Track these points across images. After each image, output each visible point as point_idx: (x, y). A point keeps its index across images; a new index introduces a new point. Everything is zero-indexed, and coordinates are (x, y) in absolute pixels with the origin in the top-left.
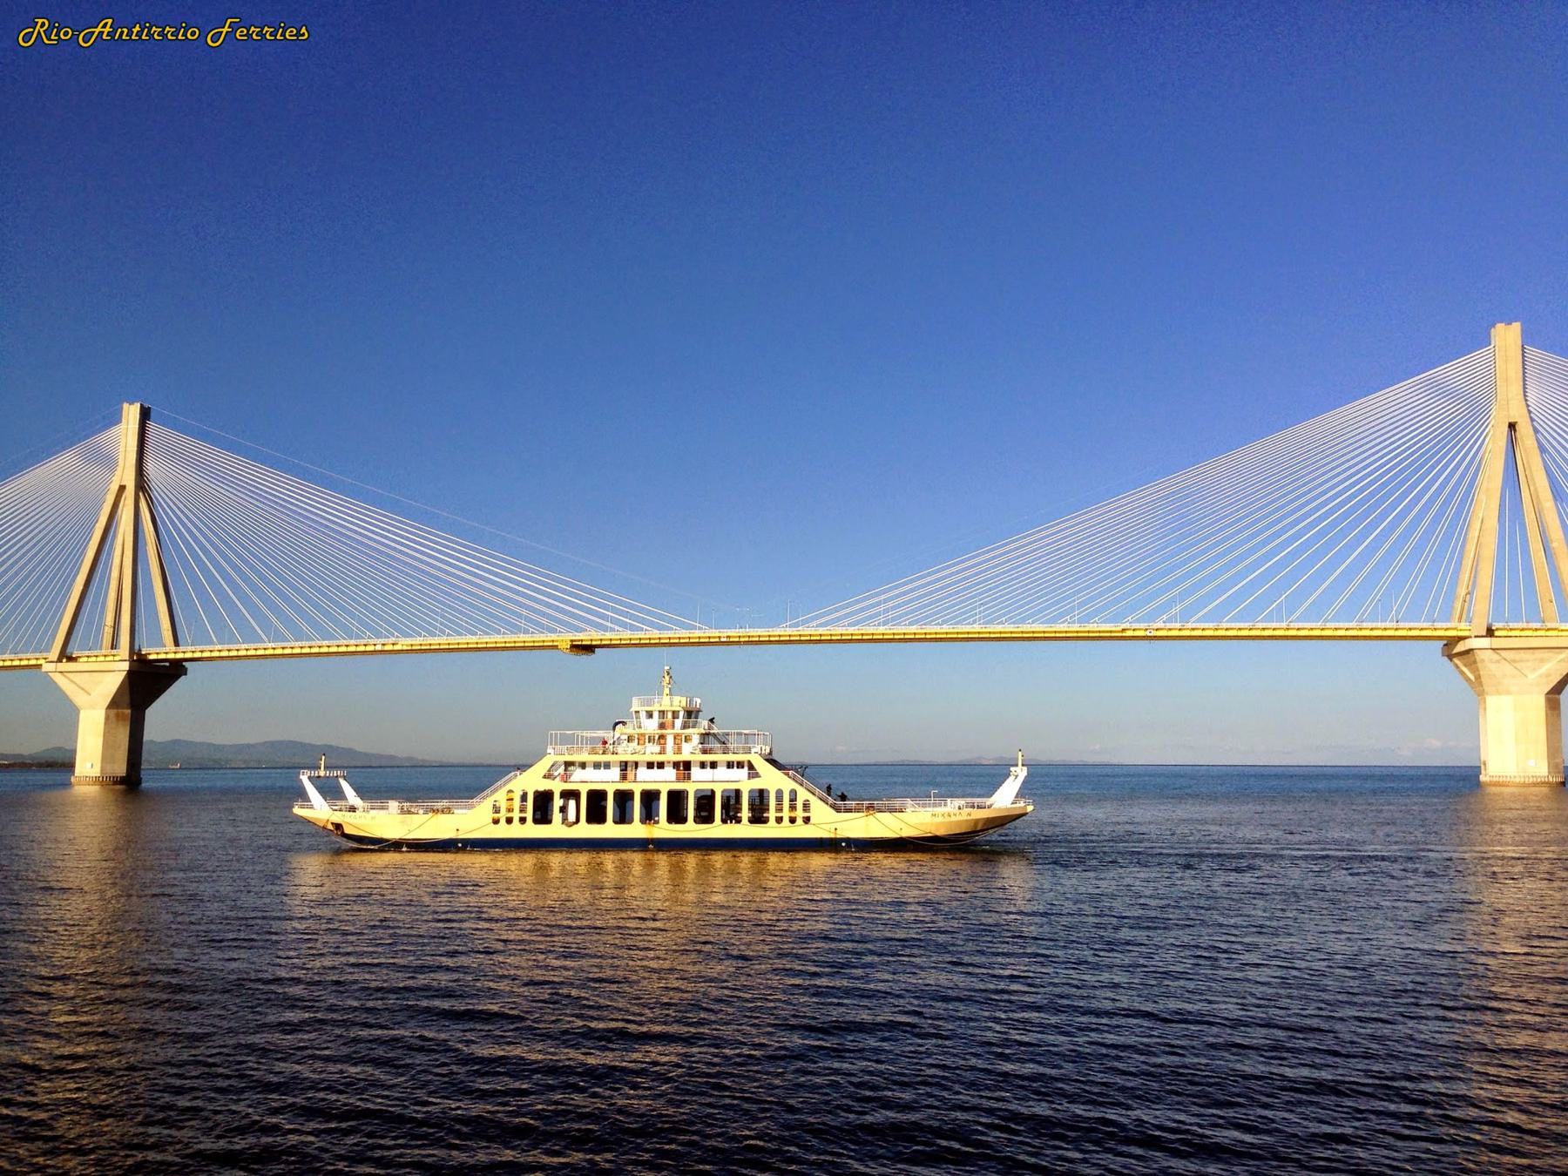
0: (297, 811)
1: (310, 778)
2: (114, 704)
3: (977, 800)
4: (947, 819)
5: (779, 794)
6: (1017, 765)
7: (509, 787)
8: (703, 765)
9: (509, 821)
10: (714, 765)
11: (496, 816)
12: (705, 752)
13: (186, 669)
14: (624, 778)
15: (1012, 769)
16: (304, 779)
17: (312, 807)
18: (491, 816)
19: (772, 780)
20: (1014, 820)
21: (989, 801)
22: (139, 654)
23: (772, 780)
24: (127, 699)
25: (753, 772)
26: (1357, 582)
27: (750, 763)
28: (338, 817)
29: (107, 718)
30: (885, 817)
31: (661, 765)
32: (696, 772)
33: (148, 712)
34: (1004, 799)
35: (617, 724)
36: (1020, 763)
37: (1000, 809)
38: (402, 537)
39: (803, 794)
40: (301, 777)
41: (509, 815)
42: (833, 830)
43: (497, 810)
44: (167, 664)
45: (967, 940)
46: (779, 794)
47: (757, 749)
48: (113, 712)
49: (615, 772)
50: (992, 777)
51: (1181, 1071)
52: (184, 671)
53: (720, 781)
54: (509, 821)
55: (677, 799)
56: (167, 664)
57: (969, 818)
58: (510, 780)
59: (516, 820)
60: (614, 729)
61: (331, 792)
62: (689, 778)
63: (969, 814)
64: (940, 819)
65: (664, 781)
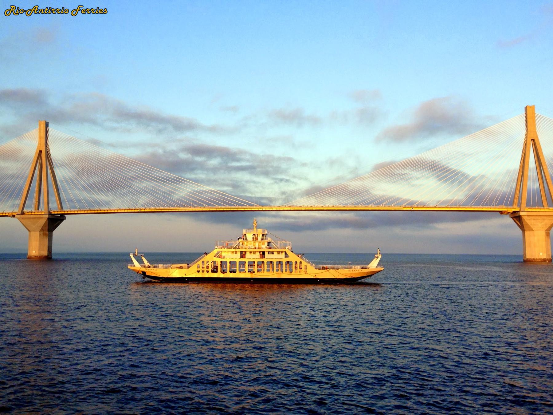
0: (129, 267)
1: (133, 256)
2: (42, 230)
3: (364, 266)
4: (354, 272)
5: (296, 262)
6: (378, 254)
7: (202, 260)
8: (269, 253)
9: (203, 271)
10: (273, 253)
11: (199, 269)
12: (270, 248)
13: (66, 217)
14: (242, 257)
15: (376, 255)
16: (132, 256)
17: (134, 266)
18: (196, 269)
19: (293, 258)
20: (377, 272)
21: (368, 266)
22: (50, 212)
23: (293, 258)
24: (47, 228)
25: (286, 255)
26: (443, 171)
27: (285, 252)
28: (143, 269)
29: (40, 235)
30: (332, 271)
31: (254, 253)
32: (248, 255)
33: (54, 232)
34: (374, 265)
35: (239, 238)
36: (379, 253)
37: (372, 269)
38: (135, 167)
39: (304, 263)
40: (131, 256)
41: (203, 269)
42: (315, 276)
43: (198, 267)
44: (59, 215)
45: (137, 352)
46: (296, 262)
47: (287, 248)
48: (42, 233)
49: (258, 255)
50: (370, 258)
51: (402, 370)
52: (65, 218)
53: (275, 257)
54: (203, 271)
55: (242, 264)
56: (59, 215)
57: (361, 272)
58: (202, 257)
59: (201, 271)
60: (238, 240)
61: (140, 261)
62: (264, 257)
63: (362, 271)
64: (352, 272)
65: (256, 257)
